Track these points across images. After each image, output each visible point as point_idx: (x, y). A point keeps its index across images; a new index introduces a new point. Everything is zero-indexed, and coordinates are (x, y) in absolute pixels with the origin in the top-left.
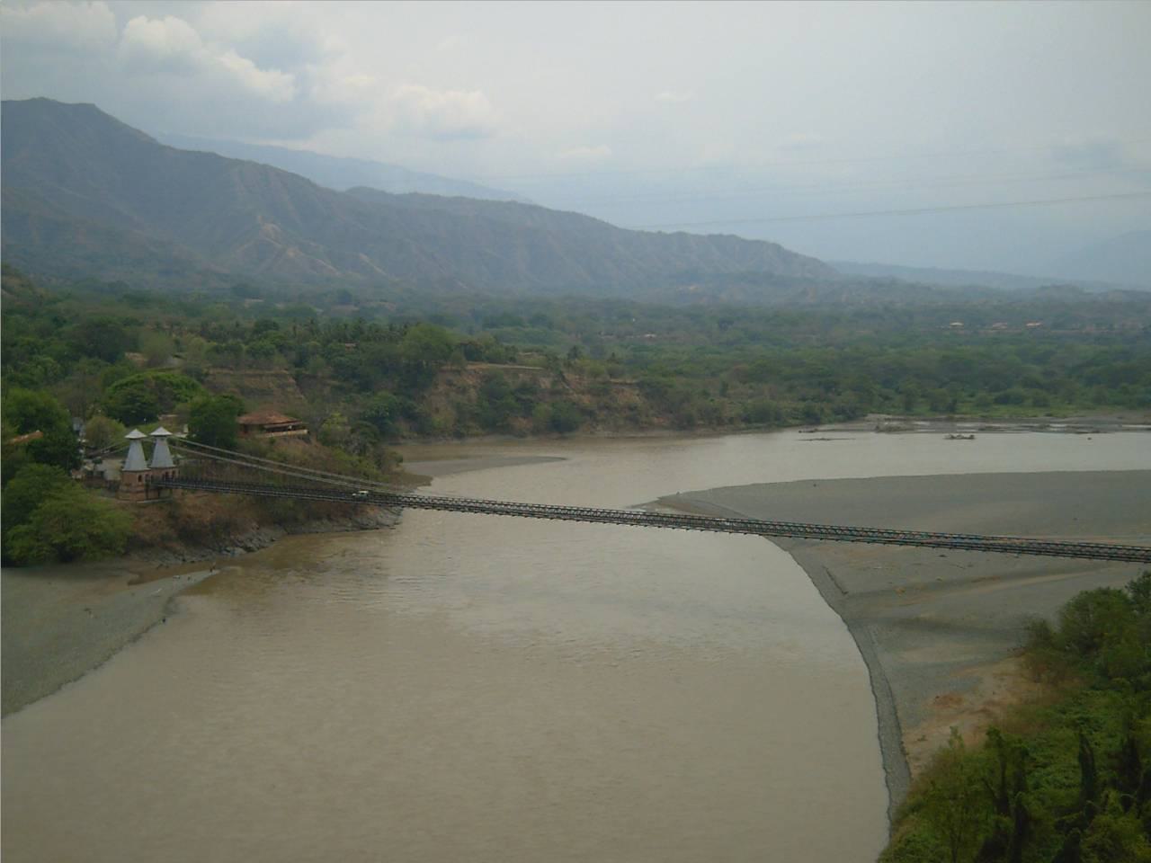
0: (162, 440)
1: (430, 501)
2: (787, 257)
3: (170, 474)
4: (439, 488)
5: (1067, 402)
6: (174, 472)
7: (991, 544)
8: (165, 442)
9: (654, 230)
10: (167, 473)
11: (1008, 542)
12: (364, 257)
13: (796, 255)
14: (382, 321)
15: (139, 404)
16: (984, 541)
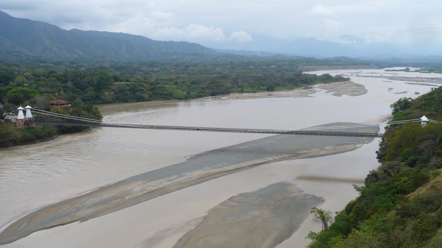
0: (29, 109)
1: (112, 125)
2: (202, 48)
3: (31, 119)
4: (264, 158)
5: (315, 91)
6: (33, 119)
7: (274, 132)
8: (29, 110)
9: (163, 40)
10: (30, 119)
11: (278, 131)
12: (76, 50)
13: (205, 47)
14: (253, 61)
15: (85, 115)
16: (271, 131)
